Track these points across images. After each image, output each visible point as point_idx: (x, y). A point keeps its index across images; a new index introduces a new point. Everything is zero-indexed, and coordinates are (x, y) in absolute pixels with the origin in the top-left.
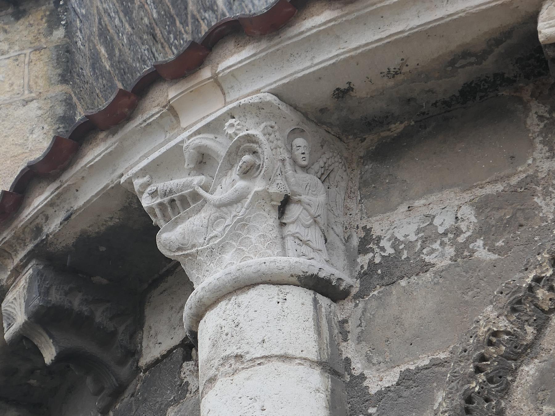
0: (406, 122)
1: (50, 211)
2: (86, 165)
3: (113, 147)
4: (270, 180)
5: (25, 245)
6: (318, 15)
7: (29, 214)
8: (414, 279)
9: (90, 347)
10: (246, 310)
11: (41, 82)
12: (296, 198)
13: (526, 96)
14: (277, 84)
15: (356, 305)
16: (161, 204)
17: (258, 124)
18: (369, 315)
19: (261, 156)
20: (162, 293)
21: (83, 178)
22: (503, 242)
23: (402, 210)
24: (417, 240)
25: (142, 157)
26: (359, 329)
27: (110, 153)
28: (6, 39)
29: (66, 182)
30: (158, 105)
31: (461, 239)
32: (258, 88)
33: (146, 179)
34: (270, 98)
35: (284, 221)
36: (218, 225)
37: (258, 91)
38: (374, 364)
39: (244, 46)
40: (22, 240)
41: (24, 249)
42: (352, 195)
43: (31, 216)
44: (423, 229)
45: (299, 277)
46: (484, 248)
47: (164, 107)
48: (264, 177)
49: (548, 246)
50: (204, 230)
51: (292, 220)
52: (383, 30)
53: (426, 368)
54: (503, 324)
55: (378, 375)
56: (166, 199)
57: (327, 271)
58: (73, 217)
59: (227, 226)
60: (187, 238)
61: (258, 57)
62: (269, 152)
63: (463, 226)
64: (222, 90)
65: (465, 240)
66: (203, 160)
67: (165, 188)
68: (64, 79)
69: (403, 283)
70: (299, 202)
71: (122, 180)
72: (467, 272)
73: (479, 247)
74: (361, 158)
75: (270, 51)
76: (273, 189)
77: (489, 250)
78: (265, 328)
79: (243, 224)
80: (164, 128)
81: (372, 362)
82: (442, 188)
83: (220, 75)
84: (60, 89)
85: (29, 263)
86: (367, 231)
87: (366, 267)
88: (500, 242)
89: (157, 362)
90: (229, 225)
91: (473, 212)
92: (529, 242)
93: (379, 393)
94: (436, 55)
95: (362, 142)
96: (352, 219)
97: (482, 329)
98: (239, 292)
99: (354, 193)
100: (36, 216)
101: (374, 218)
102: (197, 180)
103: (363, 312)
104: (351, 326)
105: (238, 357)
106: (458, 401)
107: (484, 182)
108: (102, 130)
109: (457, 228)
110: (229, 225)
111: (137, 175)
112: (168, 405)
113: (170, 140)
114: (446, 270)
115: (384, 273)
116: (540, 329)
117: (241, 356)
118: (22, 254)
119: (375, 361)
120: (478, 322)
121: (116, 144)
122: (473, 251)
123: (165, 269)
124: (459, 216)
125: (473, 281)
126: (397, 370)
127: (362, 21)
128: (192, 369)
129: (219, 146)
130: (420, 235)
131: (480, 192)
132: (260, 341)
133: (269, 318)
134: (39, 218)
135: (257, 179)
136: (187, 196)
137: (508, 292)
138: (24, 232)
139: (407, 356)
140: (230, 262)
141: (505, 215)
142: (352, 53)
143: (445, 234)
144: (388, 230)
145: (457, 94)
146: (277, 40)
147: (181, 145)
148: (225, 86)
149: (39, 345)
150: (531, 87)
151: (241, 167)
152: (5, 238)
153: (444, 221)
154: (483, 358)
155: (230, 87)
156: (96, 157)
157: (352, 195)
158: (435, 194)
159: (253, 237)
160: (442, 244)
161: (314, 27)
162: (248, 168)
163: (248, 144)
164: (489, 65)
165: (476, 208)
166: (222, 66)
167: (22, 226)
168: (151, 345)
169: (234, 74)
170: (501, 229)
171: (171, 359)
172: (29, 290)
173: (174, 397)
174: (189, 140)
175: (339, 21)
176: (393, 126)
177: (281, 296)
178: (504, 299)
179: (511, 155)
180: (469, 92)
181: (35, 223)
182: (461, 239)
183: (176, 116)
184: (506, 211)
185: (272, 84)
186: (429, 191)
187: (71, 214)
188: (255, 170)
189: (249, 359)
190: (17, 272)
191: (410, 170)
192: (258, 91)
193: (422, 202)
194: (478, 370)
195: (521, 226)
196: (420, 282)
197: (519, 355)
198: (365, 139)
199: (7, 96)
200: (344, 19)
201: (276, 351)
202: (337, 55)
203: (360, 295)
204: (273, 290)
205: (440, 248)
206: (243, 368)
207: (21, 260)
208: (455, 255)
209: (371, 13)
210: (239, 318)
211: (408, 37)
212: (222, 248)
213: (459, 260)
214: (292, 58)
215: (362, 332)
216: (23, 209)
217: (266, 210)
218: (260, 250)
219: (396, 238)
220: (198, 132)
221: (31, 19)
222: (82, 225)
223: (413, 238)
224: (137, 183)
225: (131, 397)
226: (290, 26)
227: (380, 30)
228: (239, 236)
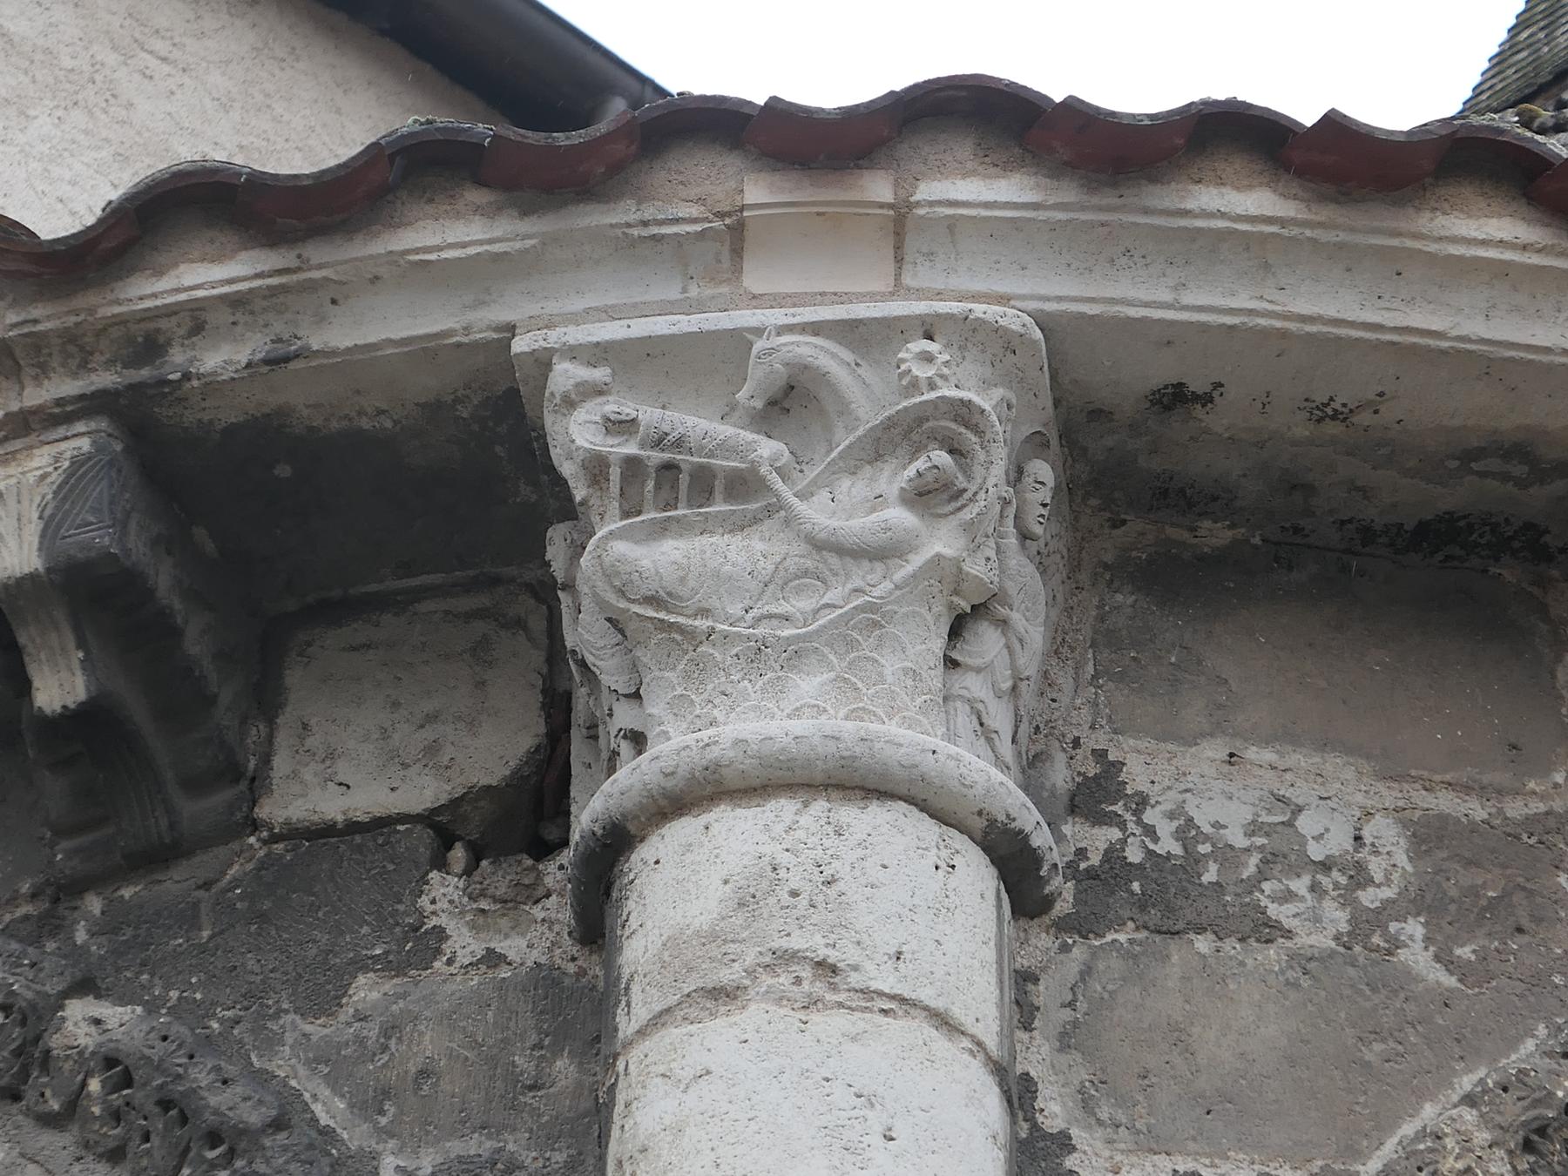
0: (1243, 530)
2: (408, 252)
3: (518, 245)
5: (84, 366)
6: (1238, 189)
7: (155, 296)
8: (1231, 946)
9: (138, 712)
10: (860, 852)
12: (1003, 611)
14: (1064, 306)
15: (1065, 948)
16: (631, 463)
18: (1099, 988)
19: (978, 471)
20: (354, 649)
21: (376, 279)
22: (1474, 951)
23: (1210, 754)
24: (1247, 850)
25: (597, 309)
26: (1067, 1014)
27: (497, 257)
29: (320, 267)
30: (700, 200)
31: (1369, 898)
32: (1018, 292)
33: (600, 374)
35: (955, 655)
36: (798, 591)
37: (1003, 299)
38: (1100, 1122)
39: (1006, 167)
40: (82, 348)
41: (74, 375)
42: (1065, 650)
43: (158, 302)
44: (1267, 829)
45: (992, 822)
46: (1426, 948)
47: (721, 215)
48: (968, 528)
50: (754, 586)
51: (978, 662)
52: (1388, 305)
55: (1107, 1153)
56: (657, 457)
58: (292, 365)
59: (827, 606)
60: (692, 583)
61: (1042, 215)
63: (1376, 868)
64: (898, 248)
65: (1378, 904)
66: (791, 402)
67: (666, 428)
69: (1203, 944)
70: (1003, 623)
71: (520, 345)
72: (1374, 990)
73: (1411, 937)
74: (1106, 566)
75: (1084, 216)
76: (976, 568)
77: (1437, 959)
78: (907, 922)
79: (873, 619)
80: (686, 265)
81: (1095, 1114)
82: (1324, 745)
83: (921, 212)
85: (79, 419)
87: (1095, 859)
88: (1467, 949)
89: (327, 831)
90: (835, 607)
91: (1402, 841)
92: (1537, 981)
94: (1457, 422)
95: (1114, 526)
96: (1057, 714)
97: (1451, 1159)
98: (834, 795)
99: (1073, 649)
100: (171, 311)
101: (1131, 742)
102: (767, 449)
103: (1082, 973)
104: (1044, 993)
105: (827, 969)
107: (1437, 778)
109: (1360, 866)
110: (835, 607)
111: (573, 353)
112: (361, 965)
113: (700, 307)
114: (1321, 960)
115: (1163, 897)
117: (834, 970)
118: (69, 387)
119: (1104, 1114)
120: (1439, 1138)
121: (533, 242)
122: (1395, 944)
123: (373, 587)
124: (1366, 833)
127: (1347, 259)
128: (456, 898)
129: (866, 394)
130: (1260, 841)
132: (892, 951)
133: (916, 901)
134: (174, 320)
135: (943, 521)
136: (720, 475)
137: (1524, 1094)
138: (100, 333)
139: (1194, 1139)
140: (814, 702)
141: (1484, 886)
142: (1292, 326)
143: (1326, 866)
144: (1169, 788)
145: (1410, 525)
147: (750, 337)
148: (912, 243)
149: (30, 649)
151: (919, 474)
152: (35, 321)
155: (925, 250)
156: (451, 246)
157: (1065, 650)
158: (1304, 751)
159: (891, 665)
160: (1314, 888)
161: (1223, 215)
162: (936, 486)
163: (953, 426)
165: (1414, 835)
166: (931, 190)
167: (114, 316)
168: (308, 774)
169: (955, 227)
170: (1472, 916)
171: (387, 843)
173: (386, 953)
174: (779, 334)
175: (1295, 231)
176: (1207, 524)
177: (945, 853)
178: (1513, 1111)
179: (1513, 740)
180: (1438, 537)
181: (152, 326)
182: (1369, 898)
183: (737, 252)
184: (1489, 876)
185: (1048, 299)
186: (1285, 736)
187: (297, 356)
188: (945, 496)
189: (857, 987)
192: (1003, 299)
193: (1268, 756)
195: (1520, 930)
196: (1249, 962)
198: (1124, 522)
200: (1308, 233)
201: (926, 995)
202: (1251, 312)
203: (1081, 925)
204: (930, 829)
205: (1308, 896)
206: (841, 1005)
207: (60, 402)
208: (1349, 934)
209: (1383, 253)
210: (836, 864)
211: (1443, 352)
212: (796, 654)
213: (1357, 949)
214: (1124, 260)
215: (1075, 1024)
216: (132, 271)
217: (935, 610)
218: (905, 718)
219: (1191, 820)
220: (815, 328)
222: (295, 395)
223: (1240, 841)
224: (565, 375)
225: (199, 887)
226: (1153, 180)
227: (1382, 303)
228: (851, 644)
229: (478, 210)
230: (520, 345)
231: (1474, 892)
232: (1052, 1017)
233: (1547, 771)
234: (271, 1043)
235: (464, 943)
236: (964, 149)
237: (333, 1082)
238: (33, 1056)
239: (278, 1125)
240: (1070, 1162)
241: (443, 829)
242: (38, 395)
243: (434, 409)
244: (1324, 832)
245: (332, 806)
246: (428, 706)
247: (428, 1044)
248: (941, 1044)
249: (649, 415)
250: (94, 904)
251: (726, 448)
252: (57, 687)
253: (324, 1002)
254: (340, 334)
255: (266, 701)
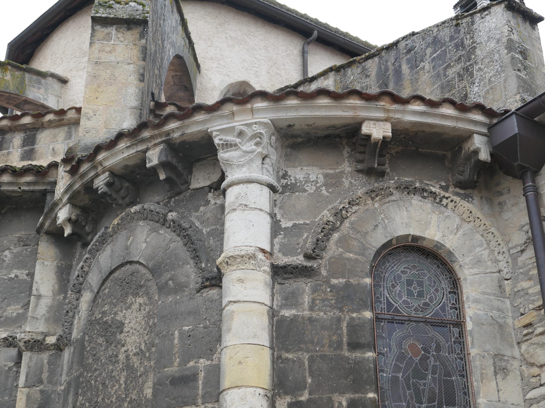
1: (175, 130)
4: (263, 148)
8: (301, 193)
9: (174, 177)
11: (135, 58)
13: (344, 143)
16: (222, 144)
17: (264, 129)
28: (123, 37)
31: (318, 185)
32: (266, 117)
34: (270, 122)
39: (264, 101)
49: (348, 197)
53: (302, 224)
54: (331, 219)
56: (225, 143)
57: (275, 184)
62: (265, 140)
63: (319, 181)
66: (241, 134)
68: (144, 59)
69: (297, 194)
71: (209, 131)
76: (264, 152)
79: (252, 160)
82: (313, 166)
84: (142, 63)
86: (286, 172)
89: (197, 189)
92: (340, 193)
93: (285, 228)
100: (170, 130)
102: (238, 140)
104: (277, 202)
105: (246, 205)
106: (315, 240)
108: (203, 110)
109: (317, 181)
111: (215, 131)
112: (201, 206)
115: (292, 188)
116: (341, 223)
118: (160, 140)
122: (321, 190)
125: (320, 200)
126: (292, 222)
127: (307, 107)
129: (249, 132)
131: (325, 171)
143: (313, 182)
146: (277, 104)
150: (346, 141)
153: (313, 177)
154: (324, 228)
159: (254, 165)
164: (338, 132)
169: (259, 110)
172: (161, 153)
178: (333, 211)
180: (327, 137)
182: (318, 185)
183: (234, 116)
186: (308, 165)
190: (156, 145)
191: (303, 156)
192: (265, 118)
193: (306, 168)
194: (322, 232)
197: (334, 230)
199: (122, 59)
201: (258, 207)
203: (282, 193)
204: (259, 186)
212: (243, 166)
218: (255, 171)
220: (242, 125)
221: (133, 32)
222: (185, 138)
223: (302, 180)
224: (214, 134)
228: (249, 164)
229: (203, 114)
230: (209, 131)
231: (331, 182)
232: (279, 205)
233: (342, 165)
234: (191, 216)
235: (212, 202)
236: (259, 99)
237: (198, 220)
238: (165, 220)
239: (191, 227)
240: (281, 223)
241: (210, 187)
242: (157, 141)
243: (202, 138)
244: (313, 177)
245: (198, 186)
246: (208, 172)
247: (208, 215)
248: (260, 213)
249: (224, 138)
250: (173, 200)
251: (233, 141)
252: (162, 177)
253: (197, 210)
254: (189, 131)
255: (191, 172)
